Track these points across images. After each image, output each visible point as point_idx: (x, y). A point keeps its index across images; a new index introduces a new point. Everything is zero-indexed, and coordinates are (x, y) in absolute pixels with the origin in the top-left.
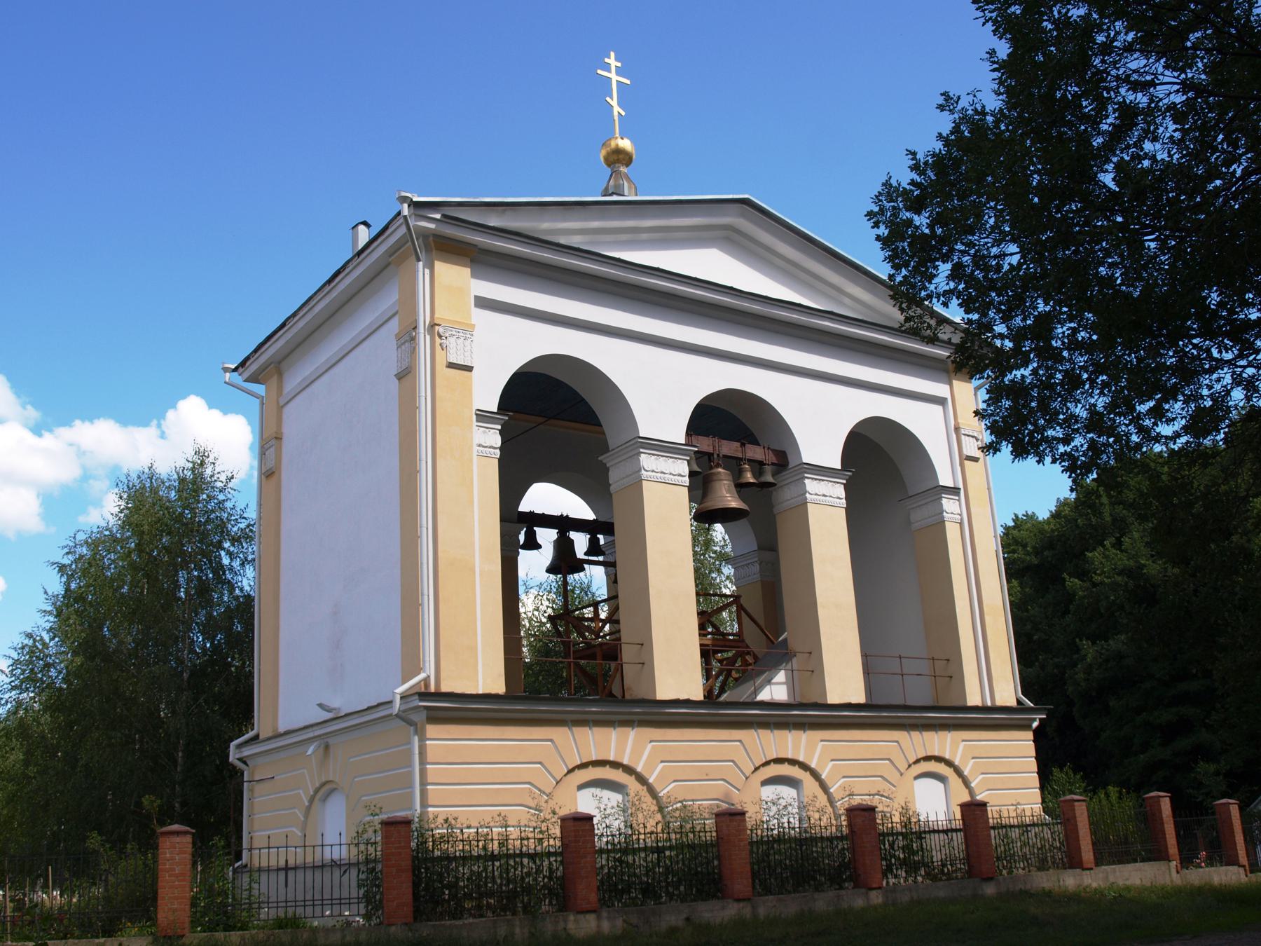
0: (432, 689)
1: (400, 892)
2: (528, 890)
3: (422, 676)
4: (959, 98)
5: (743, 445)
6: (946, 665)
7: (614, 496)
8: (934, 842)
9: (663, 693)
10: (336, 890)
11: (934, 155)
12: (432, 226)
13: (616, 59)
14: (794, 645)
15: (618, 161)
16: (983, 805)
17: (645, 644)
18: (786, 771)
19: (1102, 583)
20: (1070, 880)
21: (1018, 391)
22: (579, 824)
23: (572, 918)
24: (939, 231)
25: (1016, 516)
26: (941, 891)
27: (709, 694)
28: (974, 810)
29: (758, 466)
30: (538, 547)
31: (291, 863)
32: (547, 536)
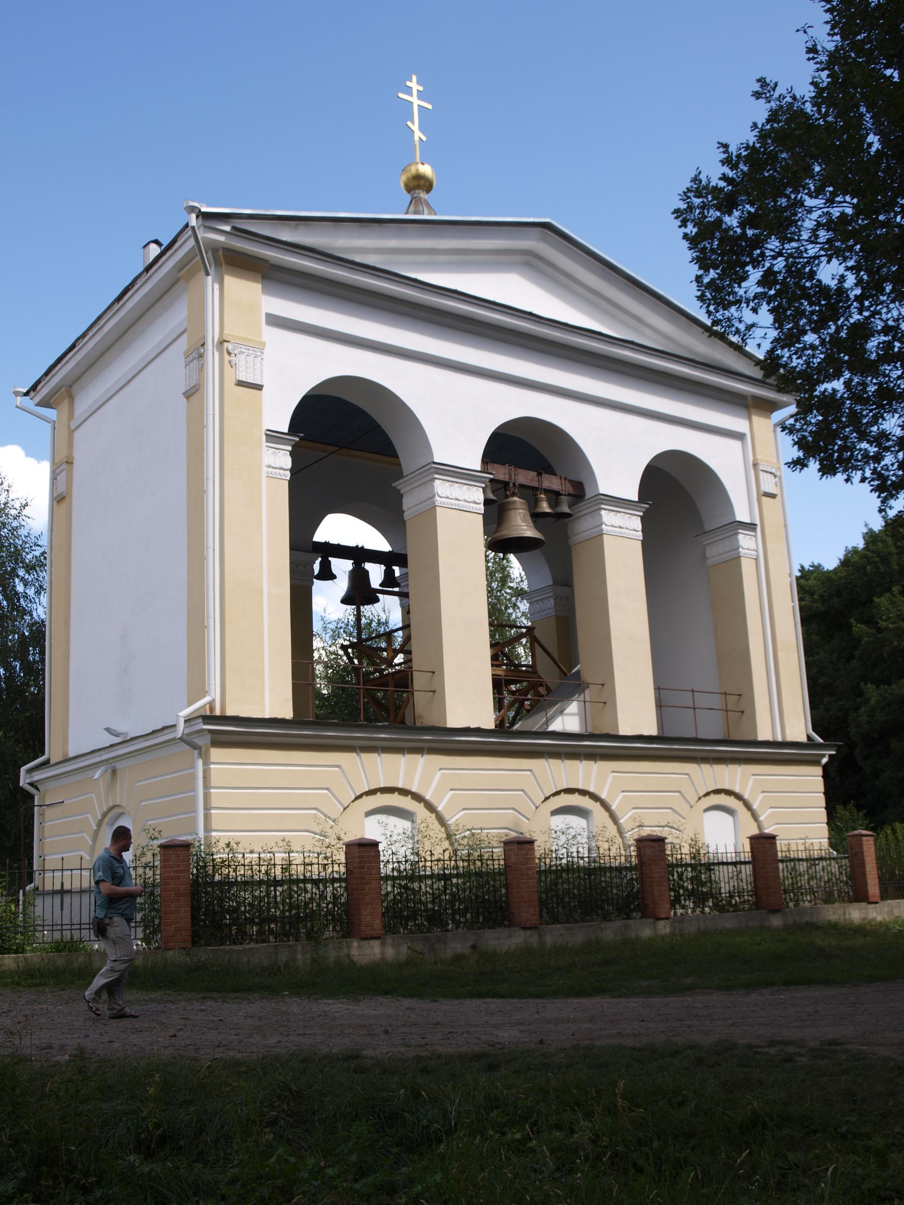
0: (218, 712)
1: (180, 915)
2: (312, 915)
3: (207, 699)
4: (776, 85)
5: (539, 474)
6: (737, 700)
7: (408, 524)
8: (723, 875)
9: (454, 721)
11: (747, 148)
12: (221, 238)
13: (418, 83)
14: (586, 676)
15: (418, 187)
16: (772, 838)
17: (436, 672)
18: (573, 802)
19: (887, 628)
20: (856, 913)
21: (830, 403)
22: (363, 852)
23: (355, 944)
24: (750, 232)
25: (802, 567)
26: (729, 922)
27: (500, 724)
28: (763, 844)
29: (554, 496)
30: (332, 577)
31: (67, 887)
32: (342, 567)
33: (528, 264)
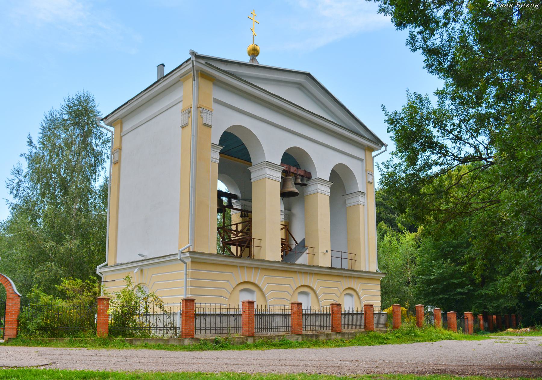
10: (204, 325)
33: (299, 88)
